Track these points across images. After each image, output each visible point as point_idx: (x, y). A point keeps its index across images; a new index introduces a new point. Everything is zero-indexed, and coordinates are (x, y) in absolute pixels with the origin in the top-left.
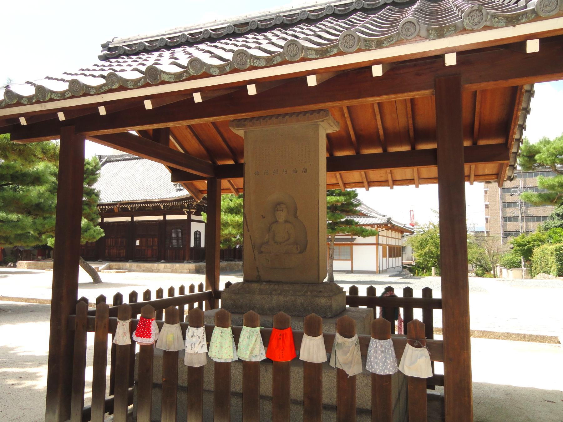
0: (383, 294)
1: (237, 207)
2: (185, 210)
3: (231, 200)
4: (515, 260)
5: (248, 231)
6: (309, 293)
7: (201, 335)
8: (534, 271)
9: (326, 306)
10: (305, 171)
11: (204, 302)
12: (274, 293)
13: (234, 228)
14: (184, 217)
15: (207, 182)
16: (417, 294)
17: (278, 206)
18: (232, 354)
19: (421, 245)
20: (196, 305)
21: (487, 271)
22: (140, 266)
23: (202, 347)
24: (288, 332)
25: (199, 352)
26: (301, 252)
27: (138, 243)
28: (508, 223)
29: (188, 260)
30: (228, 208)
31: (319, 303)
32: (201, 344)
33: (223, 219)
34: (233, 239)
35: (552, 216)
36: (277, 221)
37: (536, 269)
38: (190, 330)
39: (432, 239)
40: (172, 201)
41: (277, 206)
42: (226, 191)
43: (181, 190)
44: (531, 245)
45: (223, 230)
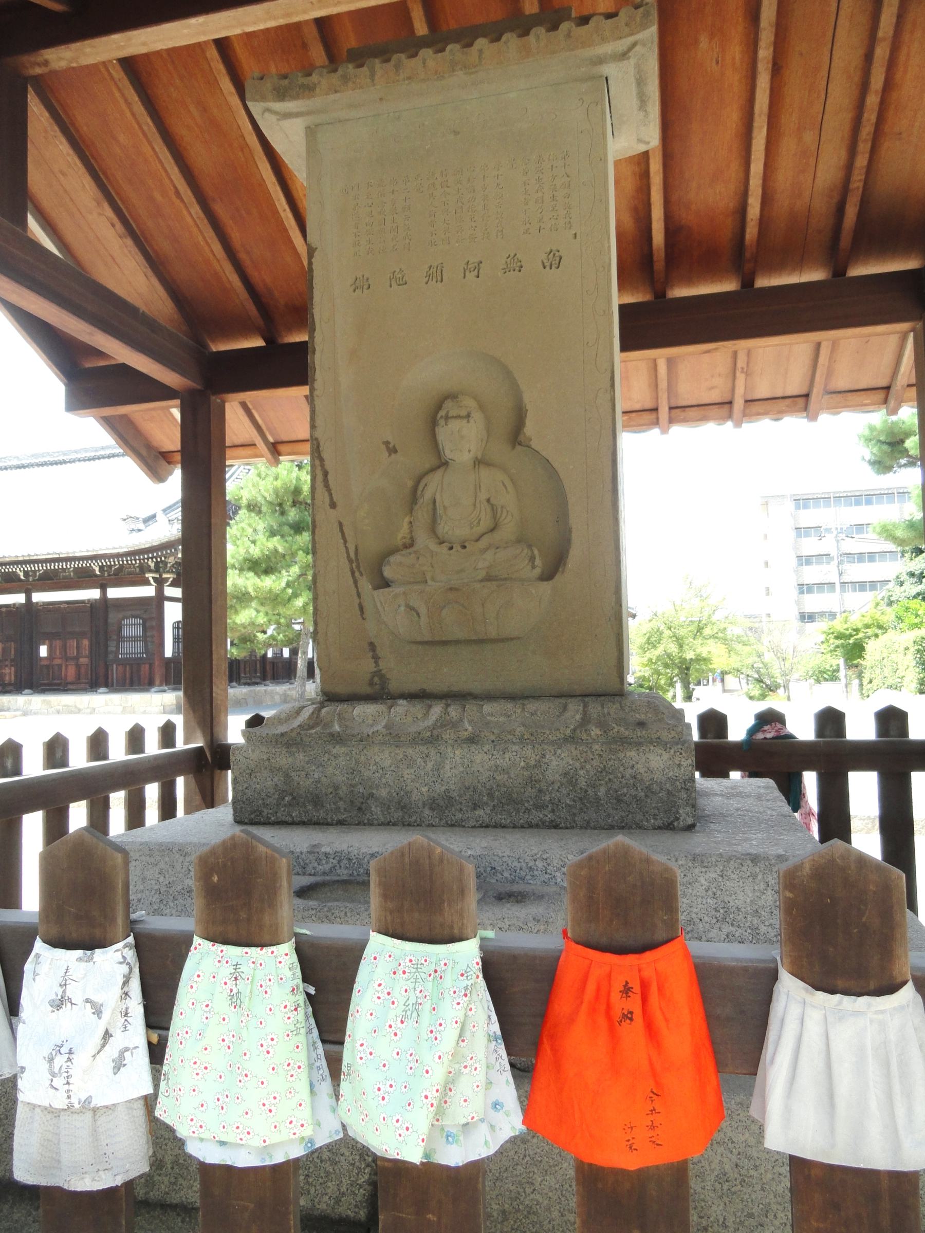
0: (752, 731)
1: (268, 558)
2: (149, 576)
3: (254, 542)
4: (828, 667)
5: (333, 505)
6: (595, 732)
7: (110, 997)
8: (866, 686)
9: (673, 781)
10: (555, 260)
11: (180, 781)
12: (448, 735)
13: (262, 604)
14: (148, 591)
15: (176, 413)
16: (861, 728)
17: (448, 404)
18: (305, 1114)
19: (648, 642)
20: (78, 815)
21: (771, 690)
22: (49, 703)
23: (119, 1065)
24: (668, 967)
25: (97, 1102)
26: (548, 576)
27: (43, 651)
28: (806, 596)
29: (161, 685)
30: (245, 560)
31: (641, 768)
32: (112, 1050)
33: (234, 585)
34: (261, 636)
35: (898, 577)
36: (443, 464)
37: (871, 682)
38: (43, 968)
39: (670, 629)
40: (118, 556)
41: (436, 411)
42: (241, 451)
43: (140, 530)
44: (861, 635)
45: (236, 612)
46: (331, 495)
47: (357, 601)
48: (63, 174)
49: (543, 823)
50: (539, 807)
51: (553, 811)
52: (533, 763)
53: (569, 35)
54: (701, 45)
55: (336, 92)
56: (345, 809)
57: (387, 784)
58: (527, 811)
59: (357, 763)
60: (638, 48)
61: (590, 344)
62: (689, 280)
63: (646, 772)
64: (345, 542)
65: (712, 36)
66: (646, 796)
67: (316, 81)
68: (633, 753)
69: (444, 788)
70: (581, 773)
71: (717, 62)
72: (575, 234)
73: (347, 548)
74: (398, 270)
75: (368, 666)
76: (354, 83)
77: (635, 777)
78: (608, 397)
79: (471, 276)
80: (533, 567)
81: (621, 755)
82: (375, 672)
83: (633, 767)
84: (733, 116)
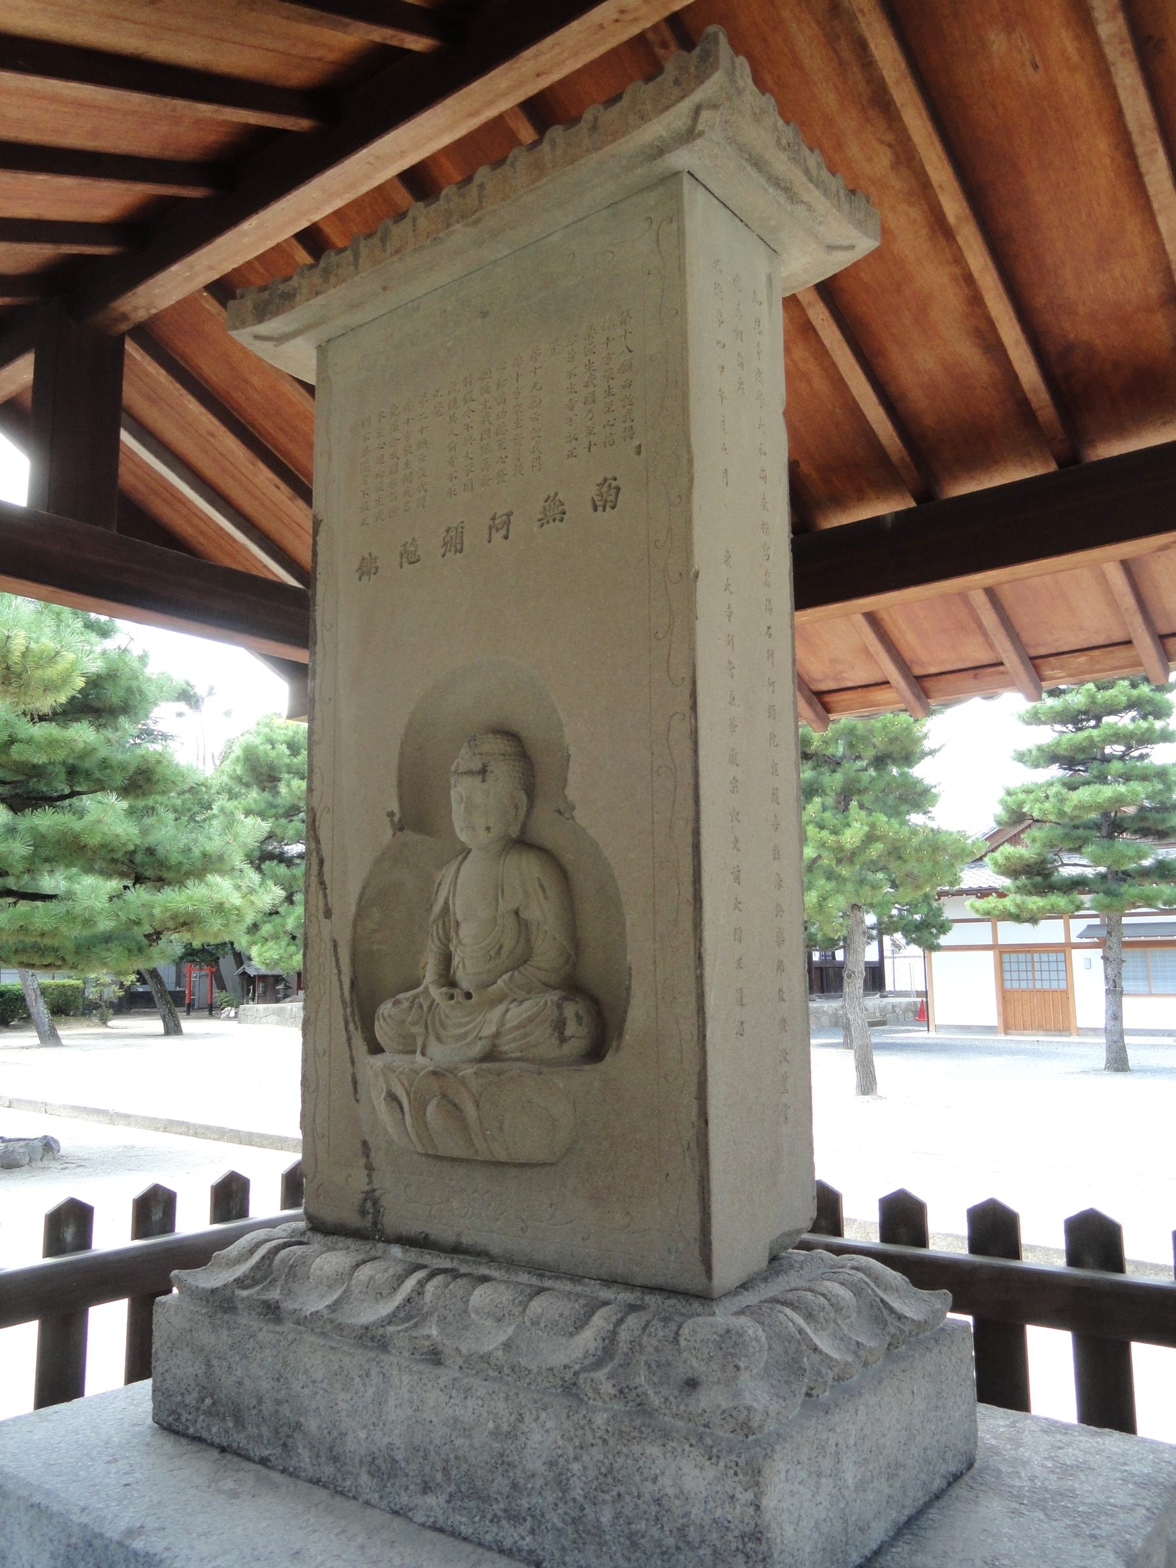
9: (723, 1527)
46: (325, 896)
47: (350, 1071)
48: (212, 435)
49: (520, 1550)
50: (515, 1518)
51: (532, 1532)
52: (505, 1428)
53: (594, 128)
54: (995, 47)
55: (317, 294)
58: (495, 1519)
59: (285, 1364)
60: (705, 115)
61: (660, 635)
62: (1121, 430)
63: (677, 1497)
64: (340, 972)
65: (1009, 28)
66: (678, 1548)
67: (296, 285)
68: (654, 1450)
69: (386, 1440)
70: (576, 1467)
71: (1036, 67)
72: (640, 446)
74: (410, 541)
75: (359, 1182)
76: (336, 275)
77: (658, 1501)
78: (686, 727)
79: (497, 536)
80: (563, 1040)
81: (636, 1449)
82: (367, 1193)
83: (655, 1480)
84: (1099, 145)
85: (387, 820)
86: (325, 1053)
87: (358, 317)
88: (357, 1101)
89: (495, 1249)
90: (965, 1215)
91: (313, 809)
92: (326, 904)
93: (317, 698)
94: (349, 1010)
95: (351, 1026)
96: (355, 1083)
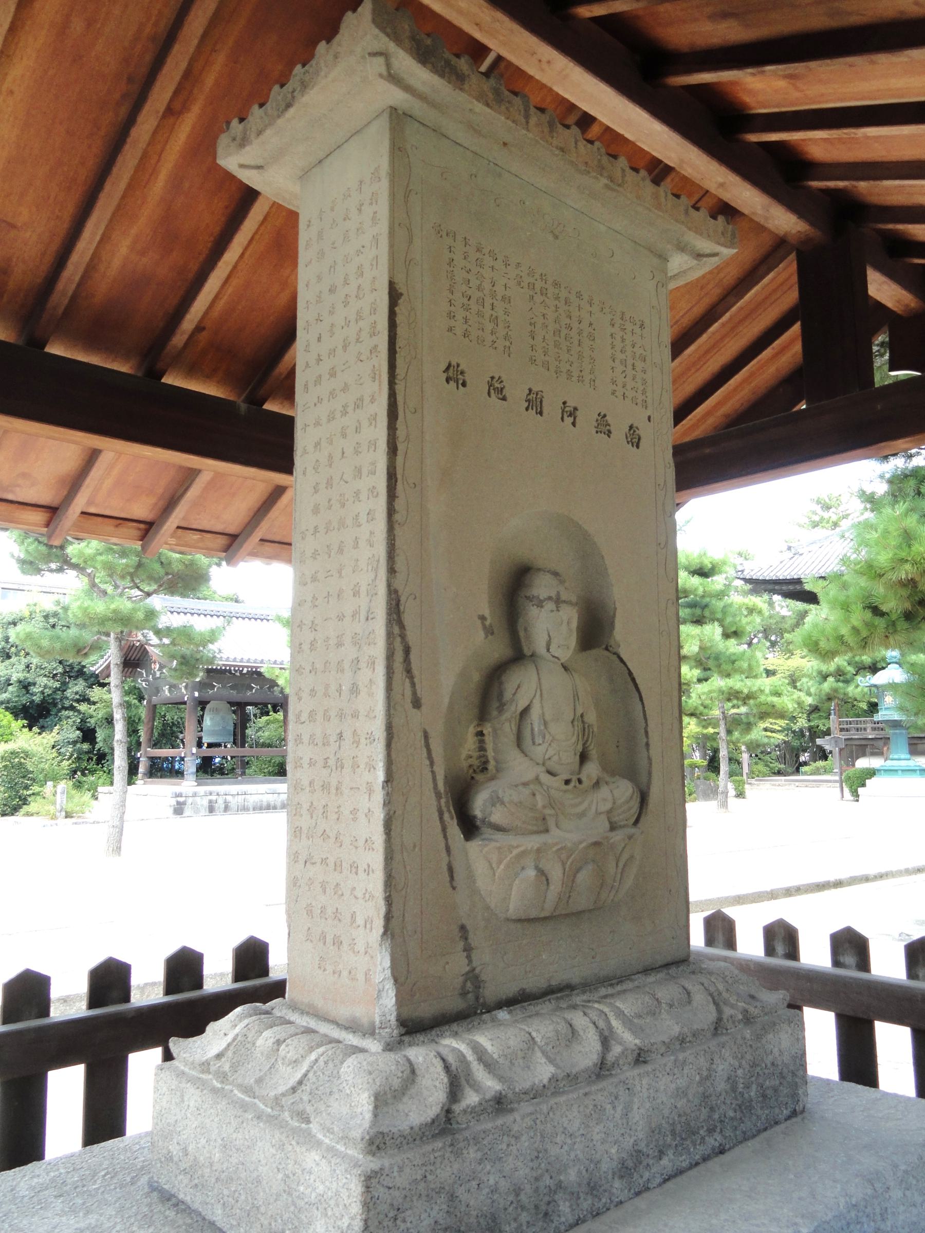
46: (413, 685)
56: (528, 1222)
57: (577, 1160)
64: (432, 763)
73: (433, 772)
75: (458, 964)
82: (467, 973)
85: (479, 622)
86: (415, 846)
87: (461, 136)
88: (454, 888)
89: (576, 980)
90: (128, 962)
91: (396, 591)
92: (414, 693)
93: (399, 476)
94: (443, 801)
95: (446, 816)
96: (451, 870)
